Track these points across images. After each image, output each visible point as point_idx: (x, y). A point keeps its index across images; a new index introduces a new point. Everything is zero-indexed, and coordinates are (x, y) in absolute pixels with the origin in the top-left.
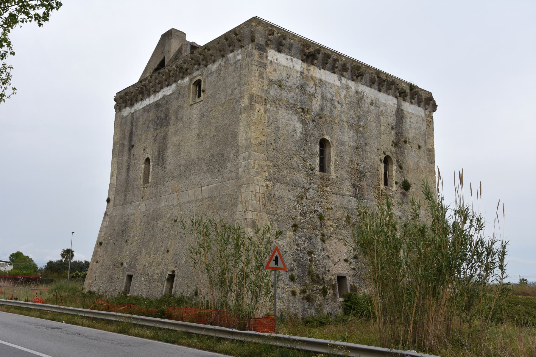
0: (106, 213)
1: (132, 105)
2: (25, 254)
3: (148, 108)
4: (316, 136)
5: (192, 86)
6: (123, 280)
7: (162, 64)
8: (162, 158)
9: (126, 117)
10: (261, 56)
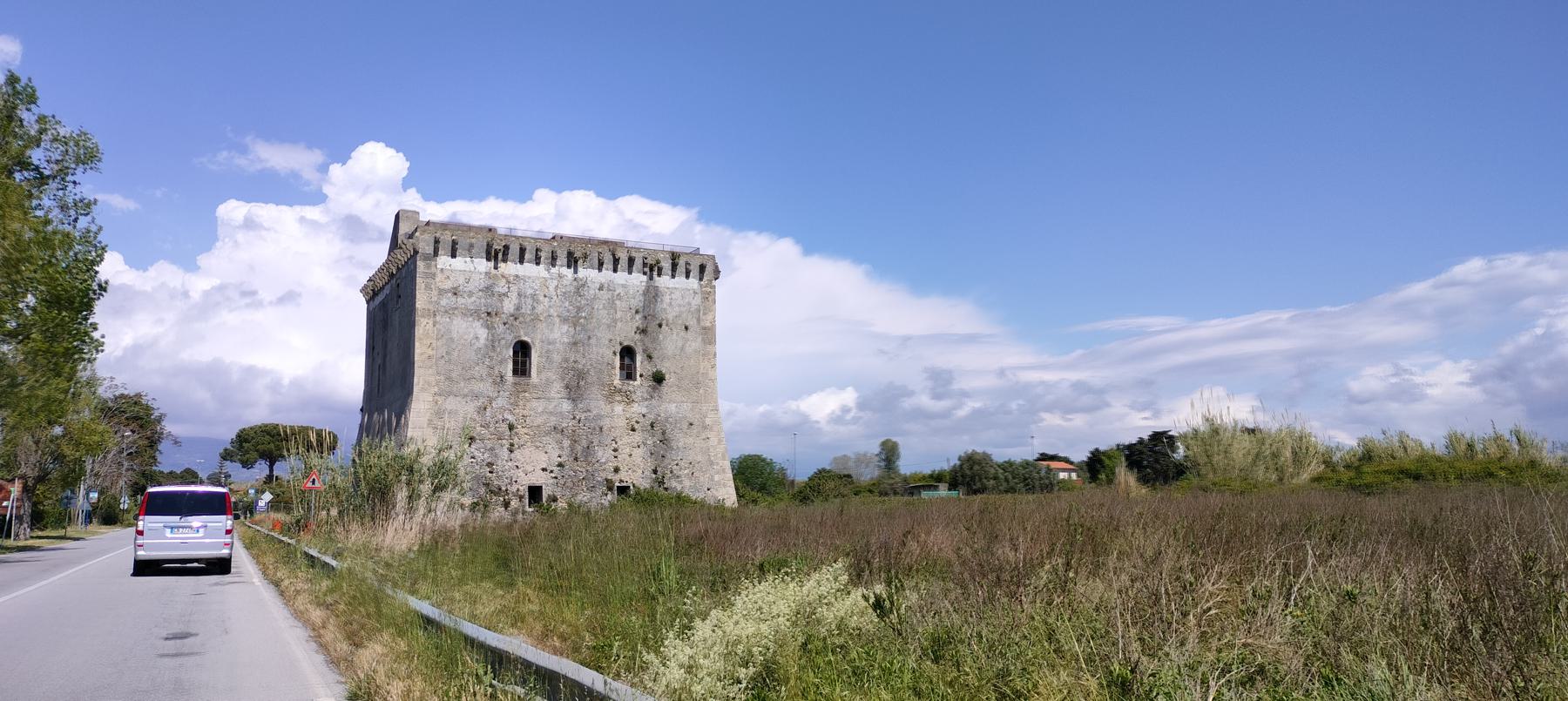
2: (284, 208)
4: (511, 339)
10: (429, 267)
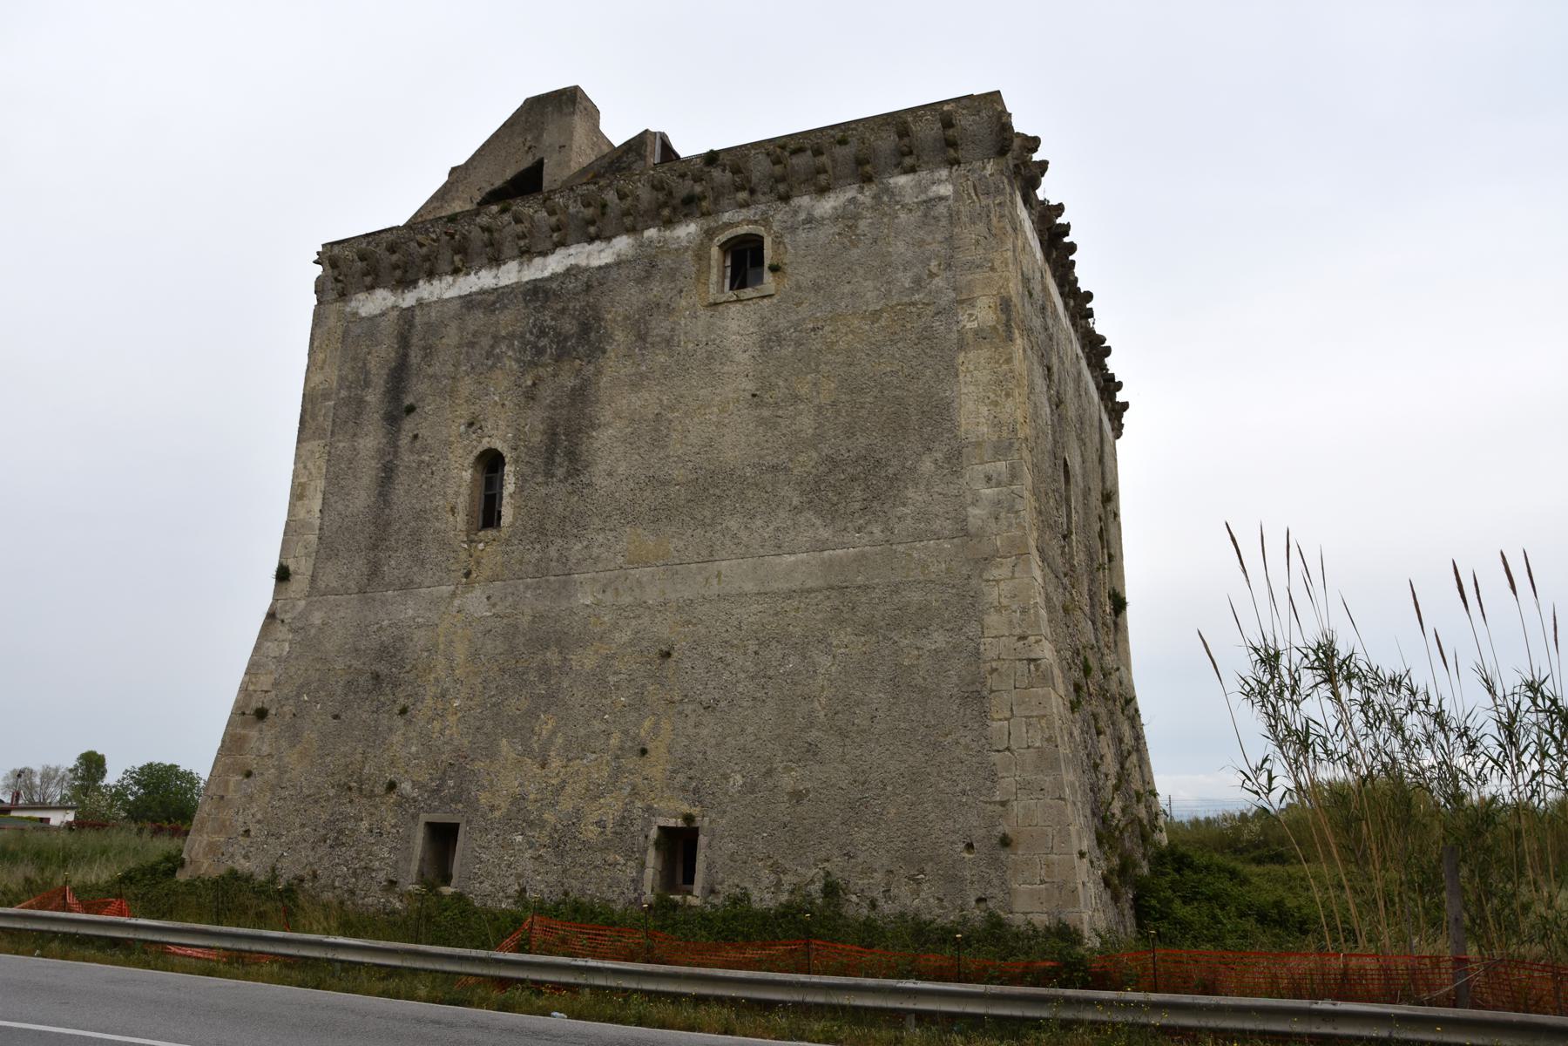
0: (271, 616)
1: (405, 283)
3: (492, 298)
5: (715, 252)
6: (408, 839)
7: (528, 182)
8: (572, 456)
9: (372, 318)
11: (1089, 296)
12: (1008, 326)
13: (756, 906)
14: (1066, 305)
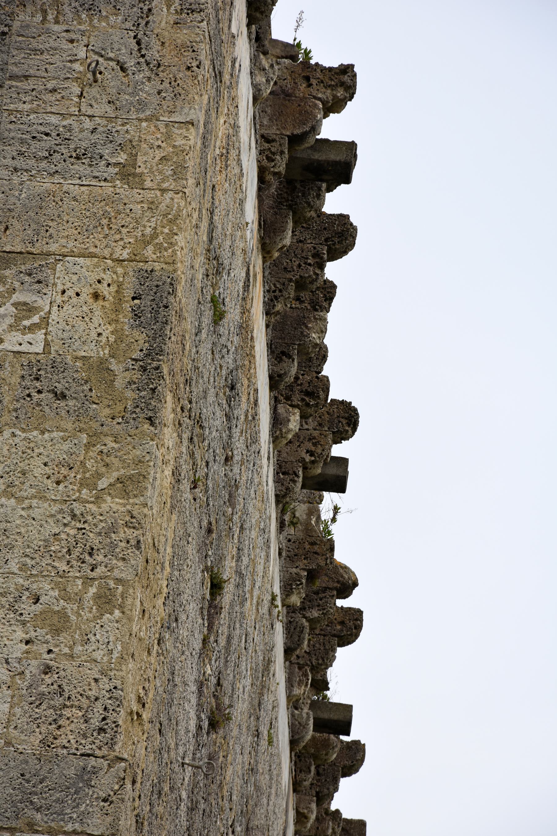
11: (346, 420)
12: (149, 365)
13: (331, 701)
14: (277, 422)
